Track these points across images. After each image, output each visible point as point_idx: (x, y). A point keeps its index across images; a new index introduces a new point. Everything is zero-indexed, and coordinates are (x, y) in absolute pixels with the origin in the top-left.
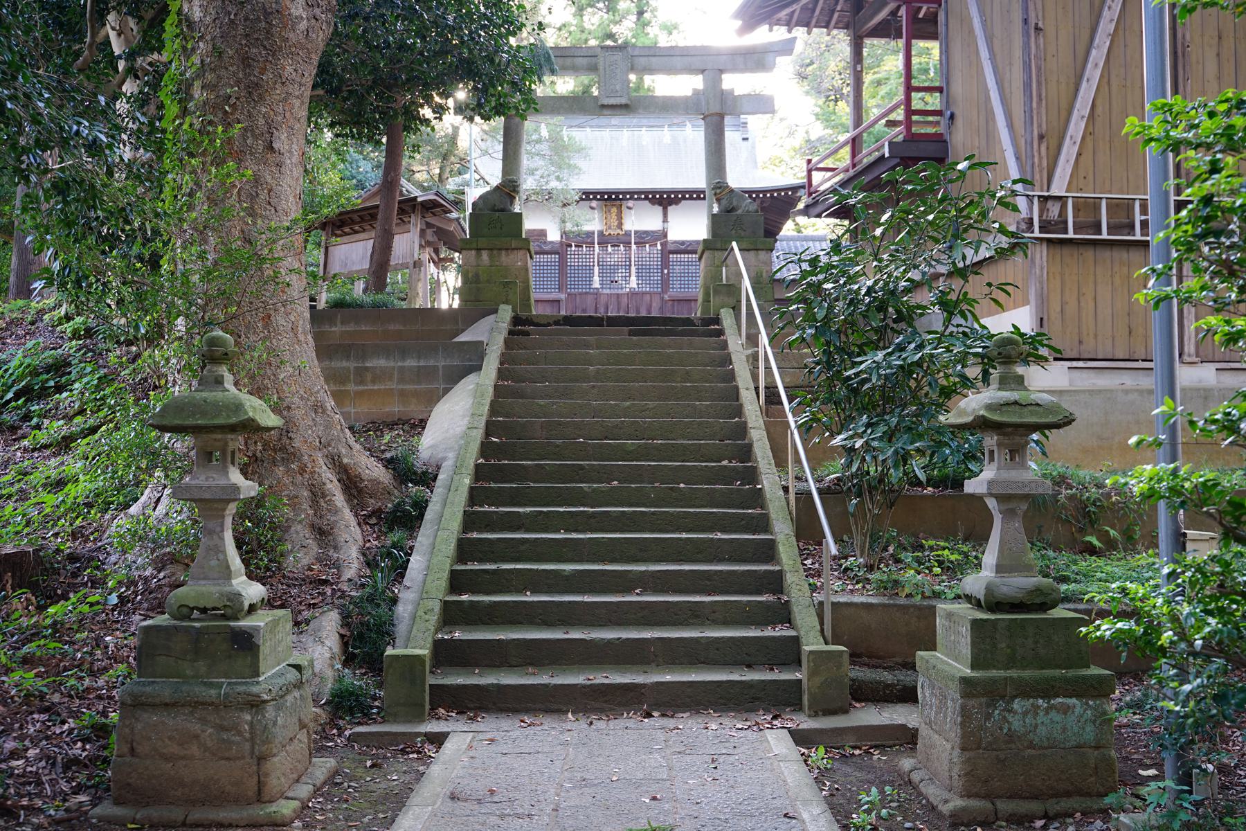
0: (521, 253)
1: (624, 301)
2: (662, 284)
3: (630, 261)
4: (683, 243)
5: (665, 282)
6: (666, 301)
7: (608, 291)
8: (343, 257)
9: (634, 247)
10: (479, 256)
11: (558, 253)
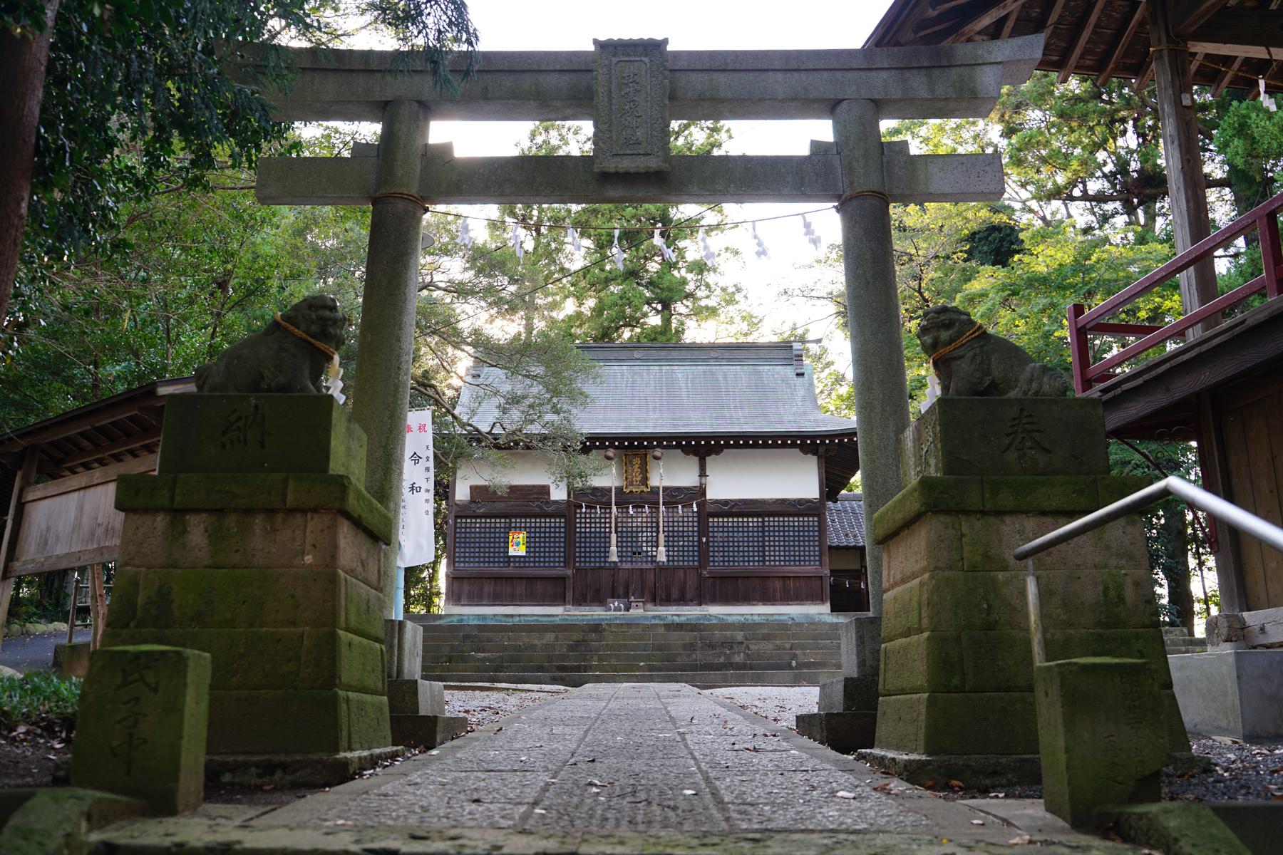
0: (315, 524)
1: (650, 578)
2: (699, 556)
3: (658, 527)
4: (726, 502)
5: (703, 553)
6: (706, 578)
7: (629, 566)
8: (43, 527)
9: (662, 508)
10: (177, 530)
11: (564, 516)
